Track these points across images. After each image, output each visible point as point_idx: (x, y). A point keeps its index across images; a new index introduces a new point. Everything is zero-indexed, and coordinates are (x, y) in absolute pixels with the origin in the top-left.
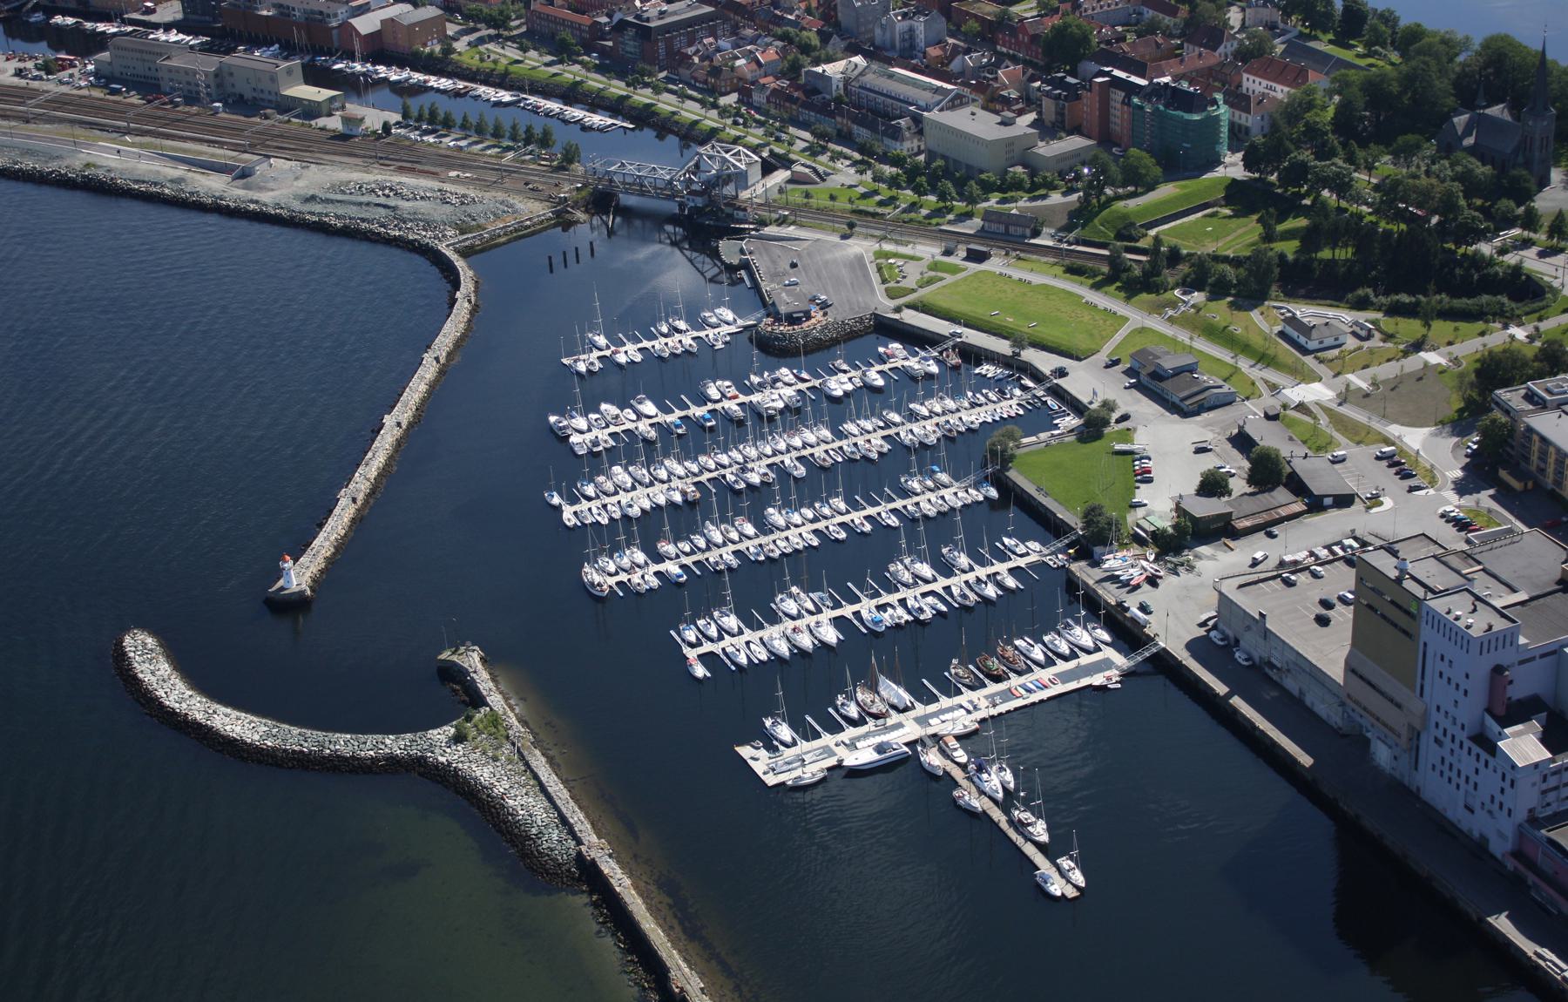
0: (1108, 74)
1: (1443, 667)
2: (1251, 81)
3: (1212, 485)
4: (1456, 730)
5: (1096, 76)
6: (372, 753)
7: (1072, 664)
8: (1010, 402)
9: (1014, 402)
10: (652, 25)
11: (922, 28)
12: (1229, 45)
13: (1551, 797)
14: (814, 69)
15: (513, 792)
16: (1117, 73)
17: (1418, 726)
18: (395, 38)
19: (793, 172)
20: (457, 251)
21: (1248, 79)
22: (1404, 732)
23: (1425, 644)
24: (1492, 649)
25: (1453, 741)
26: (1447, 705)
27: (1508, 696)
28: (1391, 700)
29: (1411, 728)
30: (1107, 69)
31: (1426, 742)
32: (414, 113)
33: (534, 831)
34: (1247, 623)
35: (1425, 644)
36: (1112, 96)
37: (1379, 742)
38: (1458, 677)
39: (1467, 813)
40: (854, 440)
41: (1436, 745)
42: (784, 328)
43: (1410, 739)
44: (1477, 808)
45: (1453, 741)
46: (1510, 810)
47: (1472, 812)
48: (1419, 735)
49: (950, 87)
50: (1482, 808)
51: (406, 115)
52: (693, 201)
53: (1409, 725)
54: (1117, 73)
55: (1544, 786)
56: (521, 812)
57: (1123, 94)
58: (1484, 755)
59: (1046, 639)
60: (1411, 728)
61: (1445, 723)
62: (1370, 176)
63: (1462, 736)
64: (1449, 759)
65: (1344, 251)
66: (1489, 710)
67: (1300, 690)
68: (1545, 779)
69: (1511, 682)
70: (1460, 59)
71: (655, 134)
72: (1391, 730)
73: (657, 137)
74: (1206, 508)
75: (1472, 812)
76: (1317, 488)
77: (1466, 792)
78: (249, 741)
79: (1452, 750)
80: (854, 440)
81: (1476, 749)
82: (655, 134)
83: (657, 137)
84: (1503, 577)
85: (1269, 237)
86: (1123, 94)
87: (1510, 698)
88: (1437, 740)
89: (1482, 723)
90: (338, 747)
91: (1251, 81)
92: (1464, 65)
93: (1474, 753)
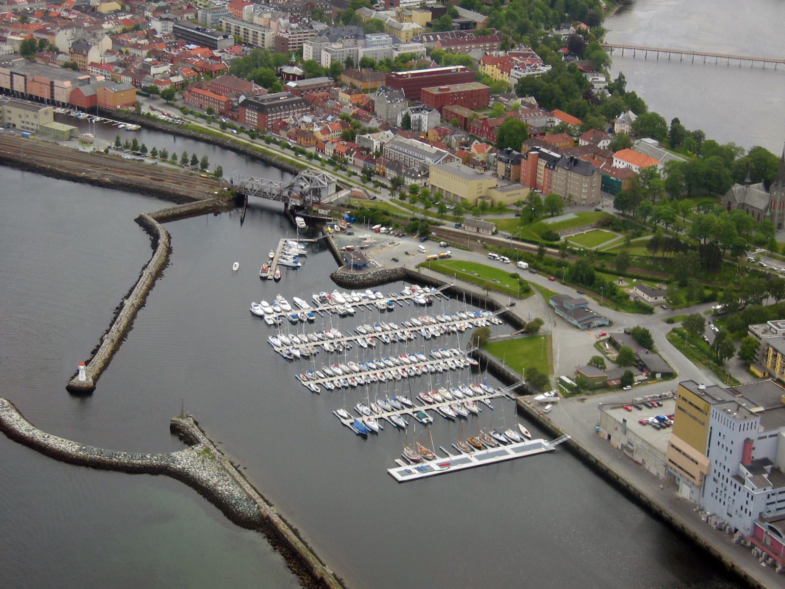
0: (537, 150)
1: (720, 439)
2: (618, 161)
3: (597, 363)
4: (724, 472)
5: (531, 151)
6: (140, 461)
7: (521, 444)
8: (482, 319)
9: (484, 319)
10: (265, 104)
11: (427, 118)
12: (605, 142)
13: (772, 507)
14: (364, 136)
15: (220, 483)
16: (543, 150)
17: (705, 473)
18: (105, 100)
19: (352, 191)
20: (156, 219)
21: (616, 161)
22: (698, 476)
23: (711, 428)
24: (746, 428)
25: (716, 497)
26: (721, 459)
27: (752, 456)
28: (693, 460)
29: (702, 473)
30: (537, 147)
31: (709, 482)
32: (123, 142)
33: (234, 502)
34: (616, 426)
35: (711, 428)
36: (539, 162)
37: (684, 484)
38: (727, 443)
39: (728, 517)
40: (396, 332)
41: (714, 482)
42: (352, 272)
43: (701, 480)
44: (733, 514)
45: (716, 497)
46: (750, 513)
47: (731, 516)
48: (705, 478)
49: (444, 151)
50: (736, 514)
51: (118, 144)
52: (295, 202)
53: (701, 472)
54: (543, 150)
55: (768, 501)
56: (226, 493)
57: (546, 162)
58: (739, 484)
59: (507, 433)
60: (702, 473)
61: (720, 469)
62: (677, 234)
63: (728, 476)
64: (720, 489)
65: (669, 254)
66: (743, 462)
67: (643, 460)
68: (768, 497)
69: (754, 448)
70: (737, 158)
71: (213, 214)
72: (692, 476)
73: (216, 215)
74: (594, 374)
75: (731, 516)
76: (652, 368)
77: (728, 505)
78: (70, 452)
79: (722, 484)
80: (396, 332)
81: (735, 481)
82: (213, 214)
83: (216, 215)
84: (752, 400)
85: (628, 245)
86: (546, 162)
87: (753, 458)
88: (714, 479)
89: (738, 469)
90: (120, 457)
91: (618, 161)
92: (739, 161)
93: (733, 484)
